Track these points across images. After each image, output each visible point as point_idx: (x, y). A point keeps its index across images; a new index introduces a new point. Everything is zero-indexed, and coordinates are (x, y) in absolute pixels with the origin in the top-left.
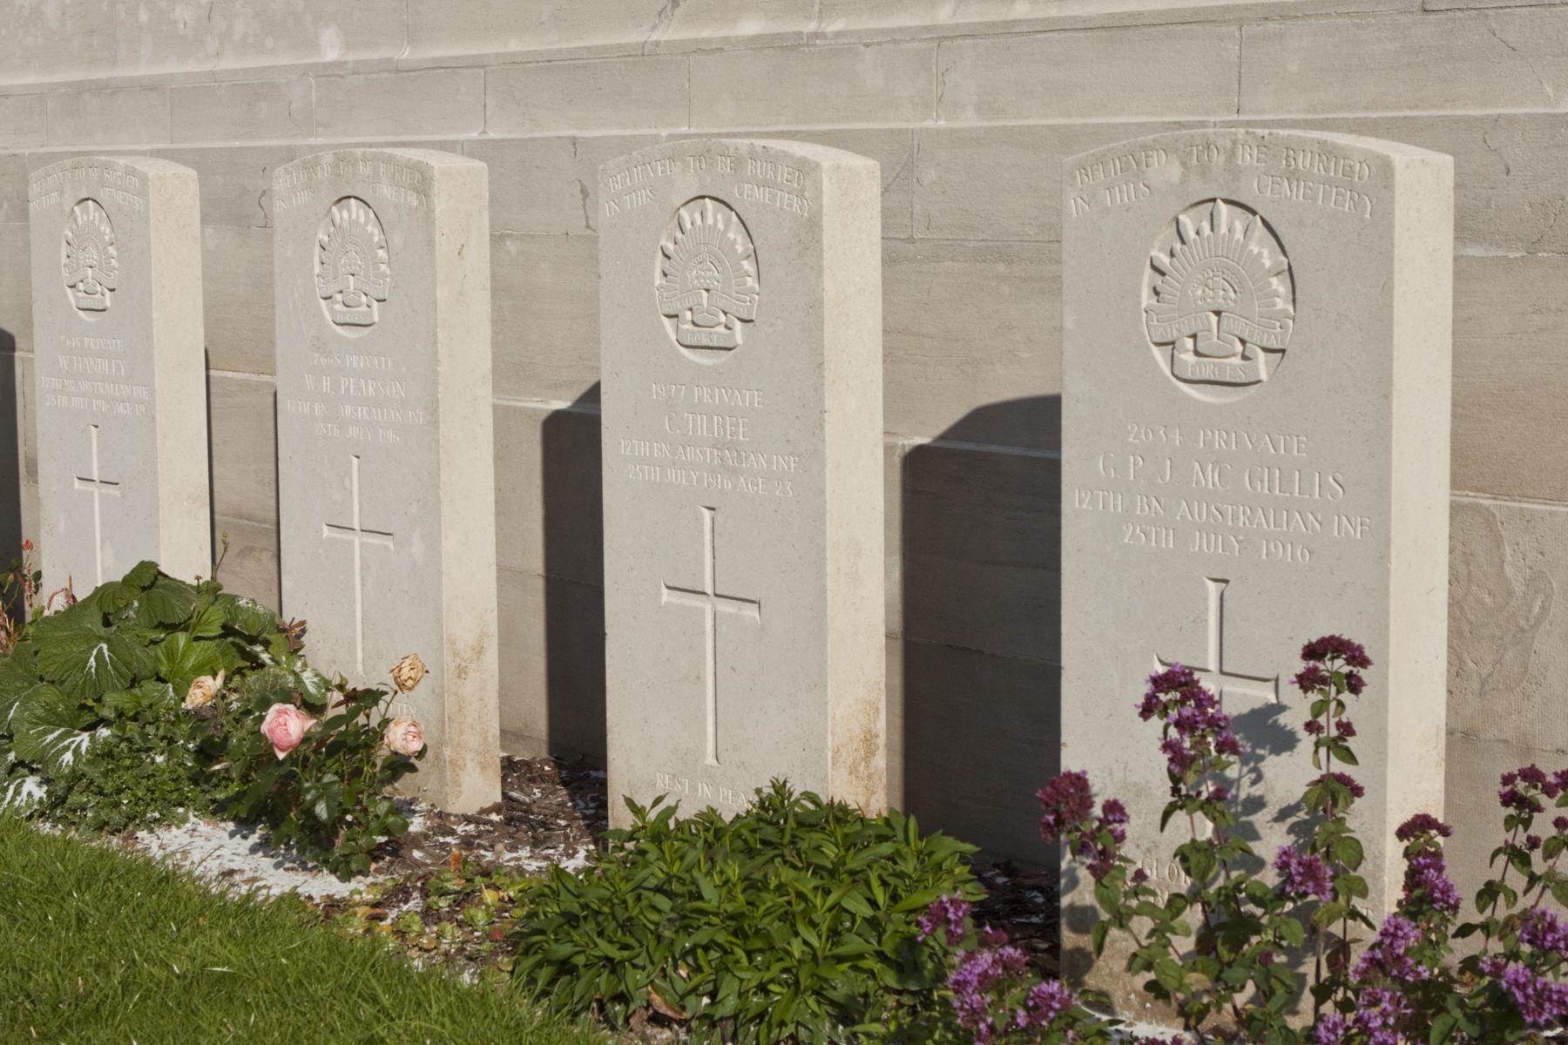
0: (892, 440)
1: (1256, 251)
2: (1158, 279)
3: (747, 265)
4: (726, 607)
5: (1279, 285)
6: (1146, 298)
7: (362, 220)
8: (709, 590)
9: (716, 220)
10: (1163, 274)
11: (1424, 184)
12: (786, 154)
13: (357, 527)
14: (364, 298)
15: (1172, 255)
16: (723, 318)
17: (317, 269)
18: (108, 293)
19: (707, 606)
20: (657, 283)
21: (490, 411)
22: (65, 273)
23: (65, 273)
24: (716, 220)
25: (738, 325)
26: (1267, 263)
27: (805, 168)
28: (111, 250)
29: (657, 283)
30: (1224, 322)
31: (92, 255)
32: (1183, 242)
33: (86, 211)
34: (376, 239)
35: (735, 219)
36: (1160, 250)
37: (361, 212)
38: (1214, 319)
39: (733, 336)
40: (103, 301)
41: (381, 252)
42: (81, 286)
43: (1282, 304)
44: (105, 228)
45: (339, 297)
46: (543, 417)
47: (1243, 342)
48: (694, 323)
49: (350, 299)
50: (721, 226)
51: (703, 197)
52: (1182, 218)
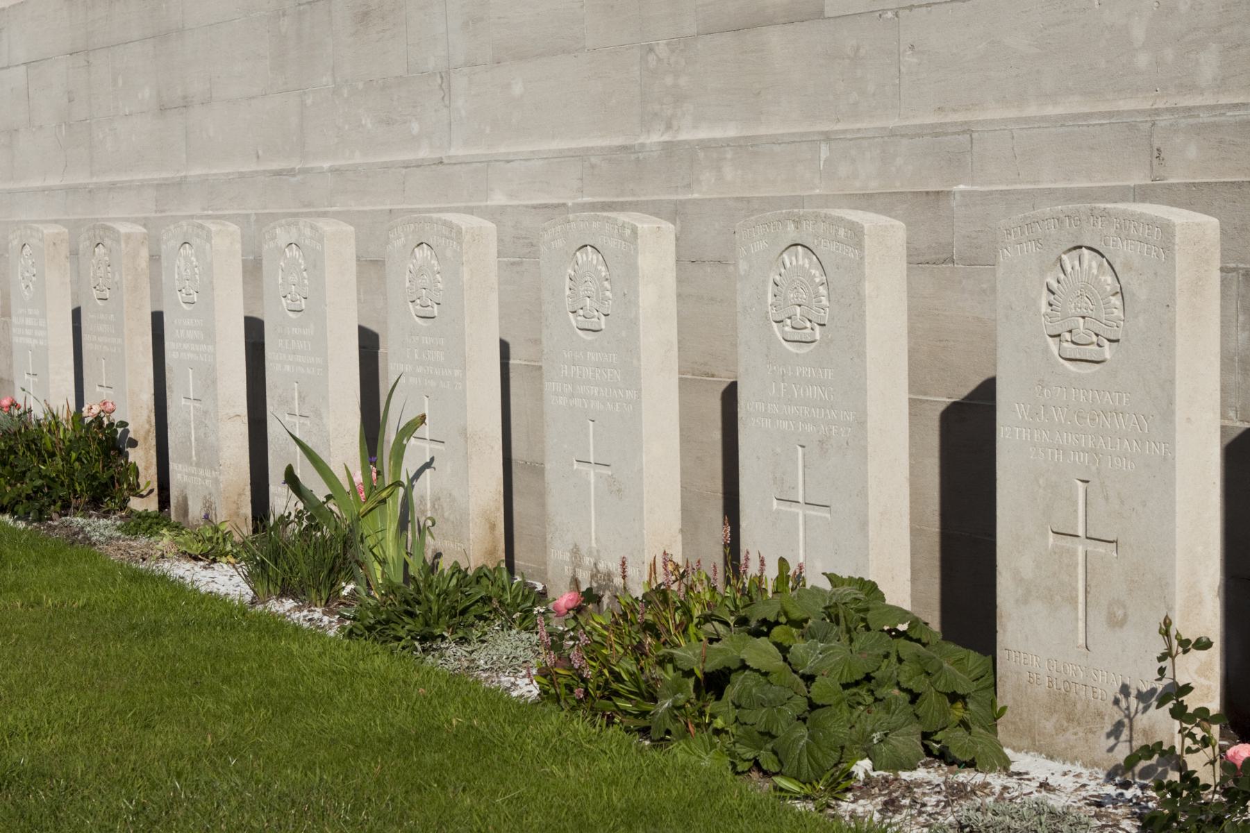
0: (1227, 422)
3: (822, 290)
4: (813, 512)
6: (1044, 308)
7: (807, 266)
8: (1081, 532)
12: (842, 219)
16: (1095, 338)
18: (817, 328)
19: (799, 511)
22: (568, 301)
23: (568, 301)
24: (1090, 267)
28: (606, 284)
31: (293, 278)
33: (291, 250)
43: (1118, 313)
44: (816, 272)
45: (581, 312)
46: (941, 408)
47: (1097, 335)
48: (1073, 342)
49: (800, 324)
51: (1080, 247)
52: (1064, 257)
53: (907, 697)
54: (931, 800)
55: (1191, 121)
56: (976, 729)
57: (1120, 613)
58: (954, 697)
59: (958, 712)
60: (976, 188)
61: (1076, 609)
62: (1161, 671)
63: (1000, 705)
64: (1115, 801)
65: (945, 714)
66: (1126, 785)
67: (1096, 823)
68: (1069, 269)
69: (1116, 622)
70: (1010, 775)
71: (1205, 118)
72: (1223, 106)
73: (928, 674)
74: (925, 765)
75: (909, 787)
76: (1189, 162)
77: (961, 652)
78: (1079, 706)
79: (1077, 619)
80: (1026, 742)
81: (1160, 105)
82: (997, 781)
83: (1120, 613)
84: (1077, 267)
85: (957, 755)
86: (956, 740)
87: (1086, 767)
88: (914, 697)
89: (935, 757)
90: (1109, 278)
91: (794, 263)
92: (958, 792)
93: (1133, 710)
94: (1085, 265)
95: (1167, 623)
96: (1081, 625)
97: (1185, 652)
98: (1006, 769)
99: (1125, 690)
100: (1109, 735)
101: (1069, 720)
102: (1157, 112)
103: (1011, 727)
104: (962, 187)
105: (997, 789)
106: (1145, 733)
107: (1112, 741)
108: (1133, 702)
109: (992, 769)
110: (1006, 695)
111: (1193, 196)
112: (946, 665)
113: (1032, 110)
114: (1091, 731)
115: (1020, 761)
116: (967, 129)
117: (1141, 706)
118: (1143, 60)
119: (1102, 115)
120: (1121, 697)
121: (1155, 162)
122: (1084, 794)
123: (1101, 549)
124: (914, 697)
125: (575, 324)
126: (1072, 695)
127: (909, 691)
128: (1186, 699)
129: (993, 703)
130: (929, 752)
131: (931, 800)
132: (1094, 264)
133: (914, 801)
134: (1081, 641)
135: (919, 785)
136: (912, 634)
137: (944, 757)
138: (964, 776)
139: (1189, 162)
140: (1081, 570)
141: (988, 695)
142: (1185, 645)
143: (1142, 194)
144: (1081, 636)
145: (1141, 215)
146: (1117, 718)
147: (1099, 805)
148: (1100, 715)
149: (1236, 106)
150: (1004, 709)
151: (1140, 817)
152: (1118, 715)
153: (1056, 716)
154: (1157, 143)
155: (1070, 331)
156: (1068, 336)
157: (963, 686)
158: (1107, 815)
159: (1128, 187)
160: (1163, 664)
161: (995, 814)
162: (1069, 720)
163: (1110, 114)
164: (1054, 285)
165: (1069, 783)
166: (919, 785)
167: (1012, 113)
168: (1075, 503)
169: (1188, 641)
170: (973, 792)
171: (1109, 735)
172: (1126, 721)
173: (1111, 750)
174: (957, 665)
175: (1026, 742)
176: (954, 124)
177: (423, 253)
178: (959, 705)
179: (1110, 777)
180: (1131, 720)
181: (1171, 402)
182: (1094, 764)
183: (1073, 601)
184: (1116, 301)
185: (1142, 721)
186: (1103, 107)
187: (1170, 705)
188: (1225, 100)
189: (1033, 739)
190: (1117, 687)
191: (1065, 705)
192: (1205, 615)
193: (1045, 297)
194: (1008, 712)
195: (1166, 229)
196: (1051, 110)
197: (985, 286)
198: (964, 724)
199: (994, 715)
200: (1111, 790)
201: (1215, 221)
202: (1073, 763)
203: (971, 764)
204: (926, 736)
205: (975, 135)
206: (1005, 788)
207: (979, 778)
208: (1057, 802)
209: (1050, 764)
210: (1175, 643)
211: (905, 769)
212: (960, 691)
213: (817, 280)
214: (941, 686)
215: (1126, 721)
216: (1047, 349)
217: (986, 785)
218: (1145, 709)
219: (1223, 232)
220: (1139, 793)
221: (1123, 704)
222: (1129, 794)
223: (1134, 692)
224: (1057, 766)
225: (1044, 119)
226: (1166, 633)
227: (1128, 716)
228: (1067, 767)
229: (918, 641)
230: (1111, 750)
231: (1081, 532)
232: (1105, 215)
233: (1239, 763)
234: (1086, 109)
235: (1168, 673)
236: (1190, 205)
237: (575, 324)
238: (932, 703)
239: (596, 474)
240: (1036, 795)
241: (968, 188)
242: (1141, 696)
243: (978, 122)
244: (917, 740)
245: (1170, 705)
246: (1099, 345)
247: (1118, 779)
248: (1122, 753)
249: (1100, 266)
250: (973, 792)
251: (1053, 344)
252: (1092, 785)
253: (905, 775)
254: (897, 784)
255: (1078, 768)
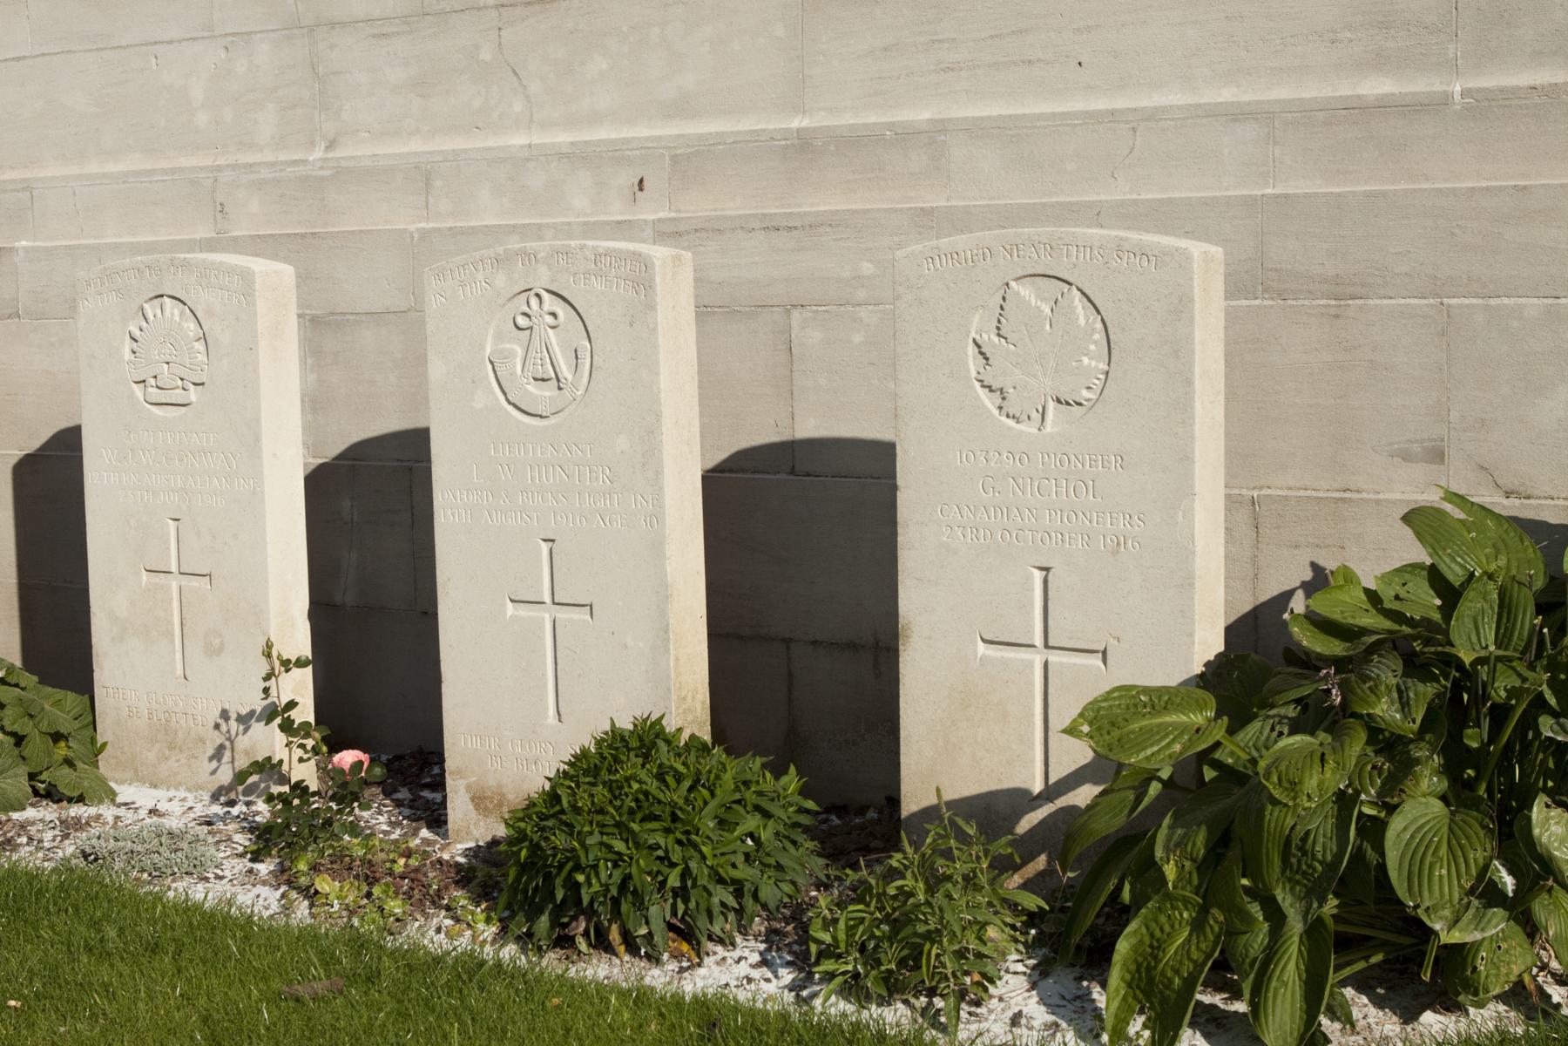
6: (128, 355)
8: (174, 568)
16: (180, 383)
43: (202, 357)
46: (14, 460)
53: (12, 740)
54: (48, 835)
55: (252, 177)
56: (80, 765)
57: (217, 642)
58: (57, 737)
59: (61, 751)
60: (38, 244)
61: (173, 641)
62: (266, 691)
63: (100, 742)
64: (224, 818)
65: (50, 754)
66: (232, 803)
67: (210, 839)
68: (151, 317)
69: (213, 651)
70: (119, 805)
71: (265, 173)
72: (282, 163)
73: (31, 716)
74: (32, 805)
75: (23, 826)
76: (251, 215)
77: (59, 694)
78: (180, 734)
79: (174, 651)
80: (128, 774)
81: (221, 161)
82: (108, 812)
83: (217, 642)
85: (66, 792)
86: (63, 778)
87: (190, 790)
88: (19, 740)
89: (41, 796)
90: (192, 325)
92: (69, 827)
93: (233, 732)
94: (167, 313)
95: (269, 645)
96: (179, 656)
97: (287, 671)
98: (113, 801)
99: (225, 715)
100: (211, 759)
101: (171, 747)
102: (219, 169)
103: (112, 761)
104: (24, 243)
105: (110, 820)
106: (247, 753)
107: (214, 764)
108: (233, 724)
109: (101, 802)
110: (105, 732)
111: (261, 245)
112: (47, 707)
113: (93, 167)
114: (193, 756)
115: (125, 793)
116: (27, 186)
117: (241, 728)
118: (202, 119)
119: (165, 171)
120: (221, 721)
121: (219, 216)
122: (192, 816)
123: (195, 582)
124: (19, 740)
126: (173, 724)
127: (13, 734)
128: (293, 714)
129: (93, 740)
130: (36, 793)
131: (48, 835)
132: (176, 312)
133: (30, 839)
134: (180, 672)
135: (33, 823)
136: (9, 680)
137: (51, 795)
138: (76, 810)
139: (251, 215)
140: (176, 604)
141: (88, 732)
142: (286, 664)
143: (208, 245)
144: (179, 666)
145: (221, 263)
146: (218, 742)
147: (209, 823)
148: (202, 741)
149: (295, 162)
150: (105, 744)
151: (251, 830)
152: (219, 739)
153: (157, 746)
154: (220, 198)
156: (153, 382)
157: (65, 724)
158: (220, 832)
159: (194, 240)
160: (267, 684)
161: (116, 840)
162: (171, 747)
163: (173, 171)
164: (137, 333)
165: (176, 808)
166: (33, 823)
167: (74, 170)
168: (167, 541)
169: (289, 661)
170: (88, 823)
171: (211, 759)
172: (227, 744)
173: (214, 772)
174: (58, 706)
175: (128, 774)
176: (14, 181)
178: (63, 744)
179: (215, 797)
180: (232, 742)
181: (257, 439)
182: (199, 787)
183: (170, 634)
184: (200, 346)
185: (243, 742)
186: (164, 164)
187: (278, 720)
188: (282, 157)
189: (136, 770)
190: (217, 713)
191: (167, 735)
192: (299, 641)
193: (128, 344)
194: (108, 747)
195: (247, 276)
196: (111, 167)
197: (53, 340)
198: (69, 762)
199: (95, 751)
200: (217, 809)
201: (290, 269)
202: (177, 789)
203: (81, 799)
204: (32, 777)
205: (35, 192)
206: (117, 818)
207: (92, 811)
208: (173, 823)
209: (154, 792)
210: (277, 663)
211: (15, 810)
212: (63, 731)
214: (44, 727)
215: (227, 744)
216: (132, 395)
217: (99, 817)
218: (246, 731)
219: (298, 276)
220: (244, 809)
221: (224, 728)
222: (235, 811)
223: (233, 716)
224: (161, 794)
225: (104, 175)
226: (269, 656)
227: (229, 739)
228: (172, 793)
229: (17, 685)
230: (214, 772)
231: (174, 568)
232: (185, 264)
233: (347, 767)
234: (149, 166)
235: (273, 692)
238: (36, 745)
240: (148, 821)
241: (30, 244)
242: (242, 719)
243: (38, 179)
244: (24, 780)
245: (278, 720)
247: (223, 799)
248: (225, 776)
249: (182, 313)
250: (88, 823)
251: (138, 390)
252: (199, 807)
253: (15, 816)
254: (10, 824)
255: (182, 794)
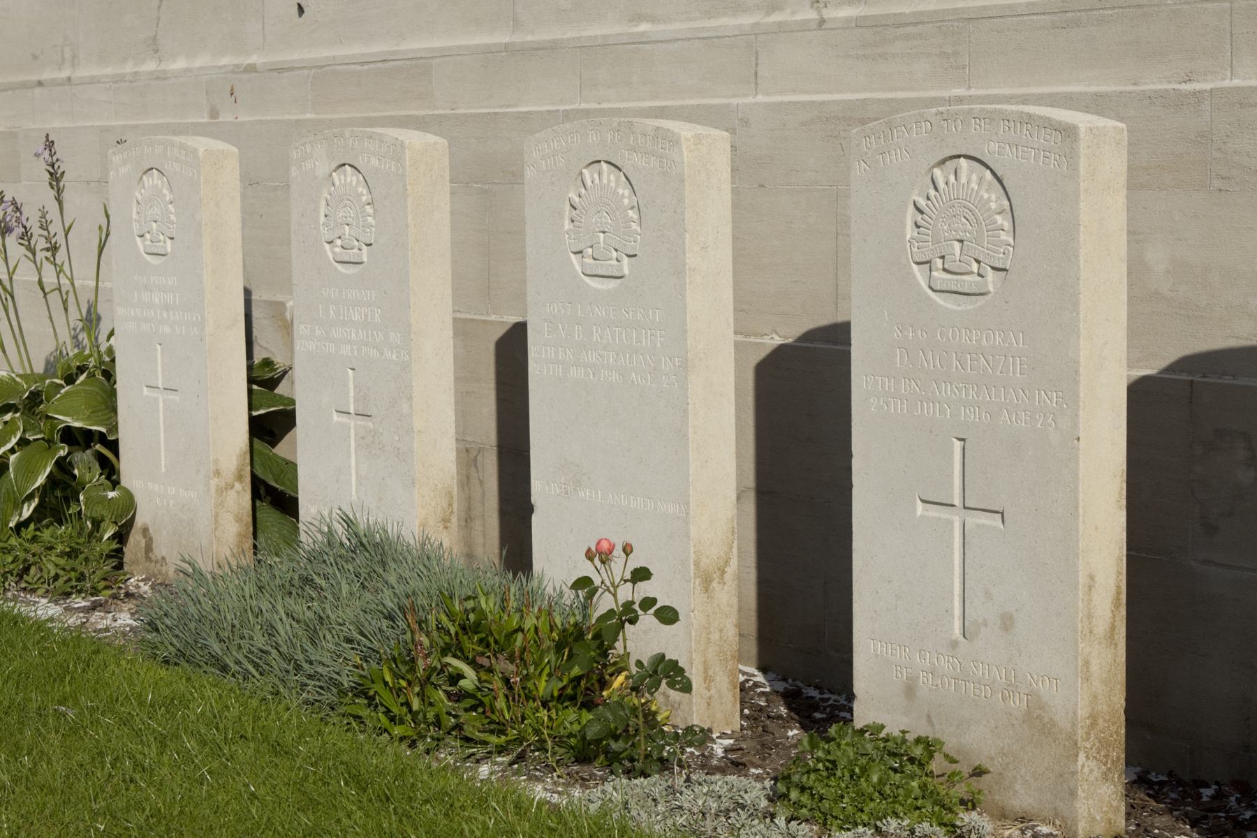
0: (458, 315)
1: (986, 196)
2: (919, 217)
3: (632, 214)
4: (975, 519)
5: (1003, 221)
6: (910, 232)
8: (957, 501)
9: (609, 181)
10: (921, 212)
11: (1104, 148)
13: (352, 411)
14: (615, 254)
15: (928, 199)
16: (975, 267)
17: (322, 219)
18: (169, 241)
20: (567, 227)
21: (731, 350)
22: (324, 230)
24: (609, 181)
25: (990, 274)
26: (993, 206)
27: (1069, 132)
28: (369, 209)
29: (567, 227)
30: (965, 248)
32: (936, 189)
34: (626, 201)
35: (623, 178)
36: (919, 195)
37: (354, 178)
38: (957, 245)
39: (986, 284)
40: (621, 268)
41: (631, 213)
42: (148, 236)
44: (362, 190)
45: (339, 242)
47: (978, 262)
48: (944, 270)
50: (613, 184)
51: (959, 156)
84: (597, 181)
91: (597, 181)
125: (331, 256)
132: (612, 178)
155: (943, 257)
164: (922, 203)
177: (154, 180)
213: (364, 198)
231: (957, 501)
236: (1087, 110)
237: (331, 256)
239: (164, 401)
246: (979, 275)
249: (617, 181)
